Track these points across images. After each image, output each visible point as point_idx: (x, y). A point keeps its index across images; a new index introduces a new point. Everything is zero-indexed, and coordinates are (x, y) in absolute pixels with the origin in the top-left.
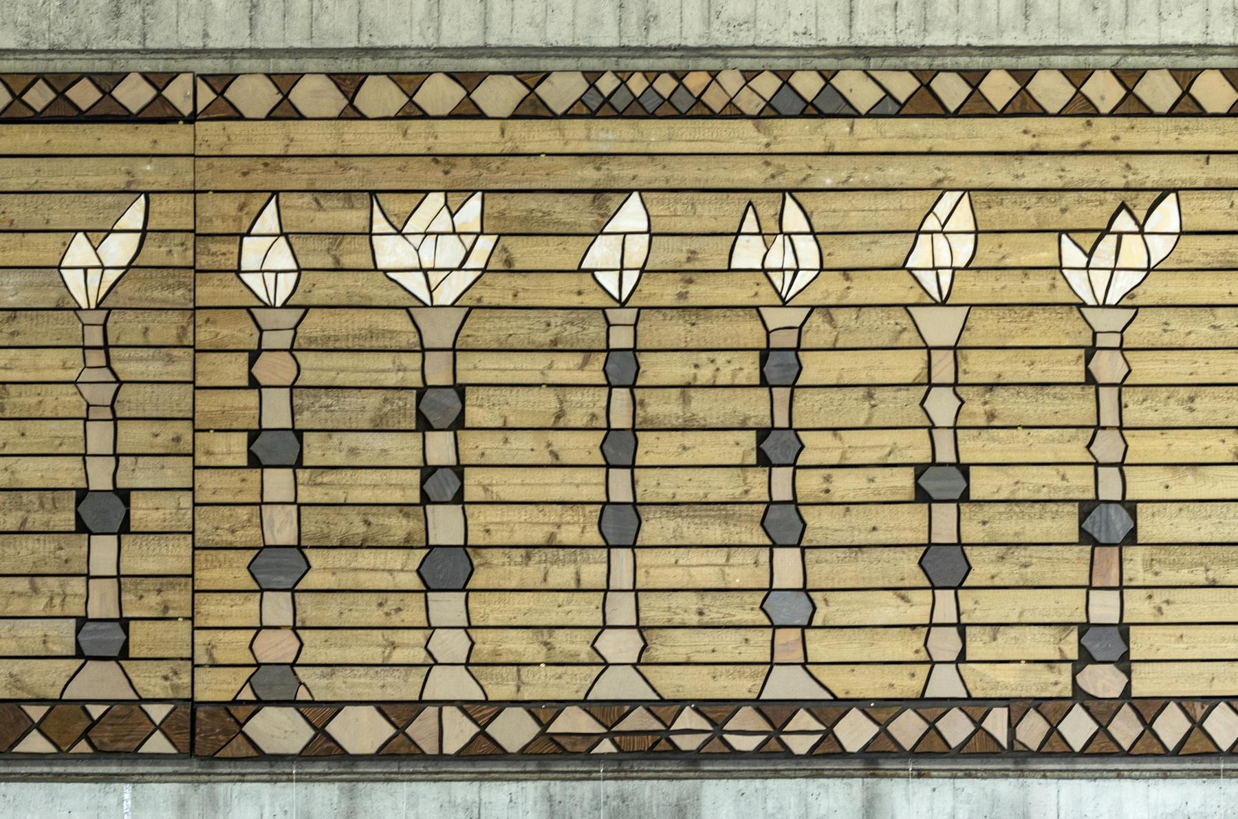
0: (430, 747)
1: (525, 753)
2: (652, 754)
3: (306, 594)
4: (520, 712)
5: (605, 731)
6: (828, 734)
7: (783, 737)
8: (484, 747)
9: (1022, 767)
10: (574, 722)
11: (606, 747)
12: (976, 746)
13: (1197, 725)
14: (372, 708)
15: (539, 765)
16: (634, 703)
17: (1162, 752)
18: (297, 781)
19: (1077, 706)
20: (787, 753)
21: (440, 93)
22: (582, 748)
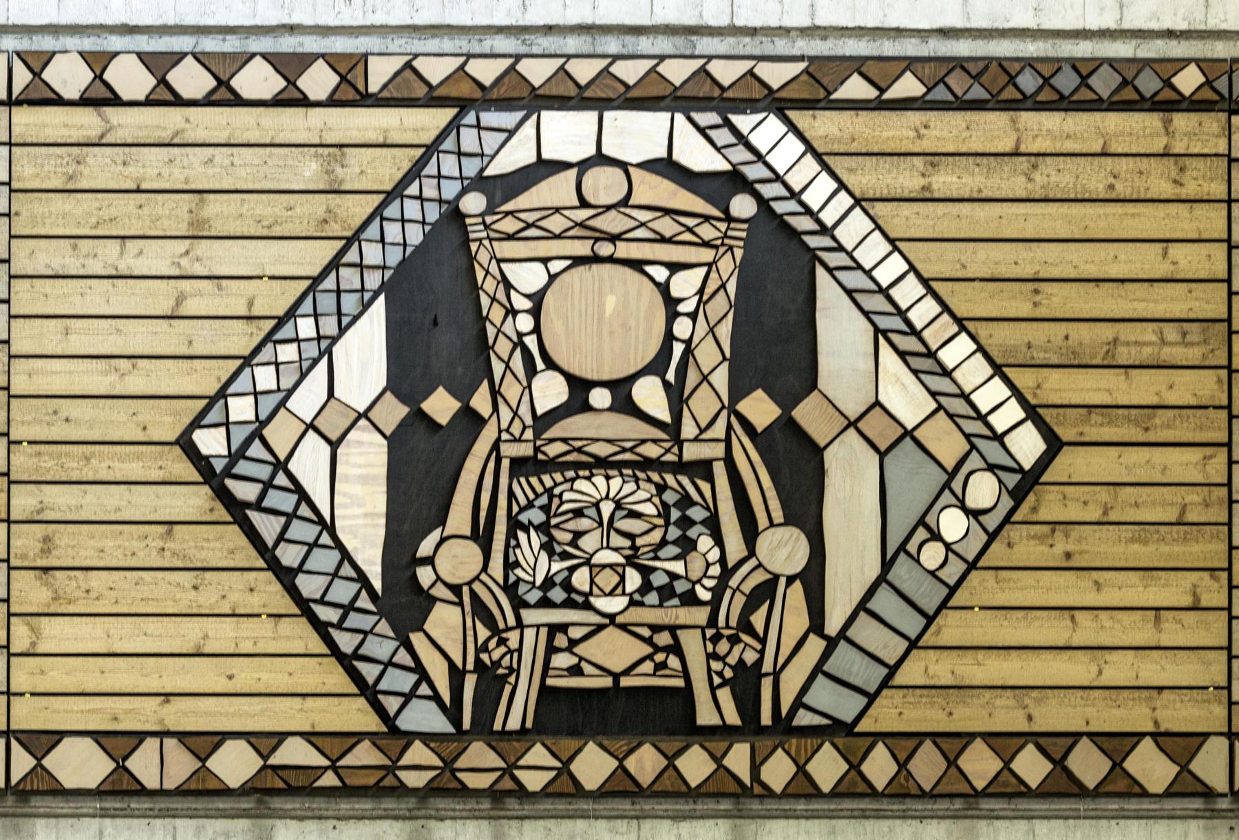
0: (151, 782)
1: (246, 790)
2: (376, 791)
3: (1084, 612)
4: (242, 744)
5: (326, 763)
6: (564, 770)
7: (516, 772)
8: (1121, 785)
9: (1212, 806)
10: (295, 753)
11: (329, 780)
12: (667, 783)
13: (1059, 763)
14: (88, 741)
15: (1206, 803)
16: (359, 736)
17: (572, 789)
18: (1084, 818)
19: (827, 744)
20: (521, 792)
21: (257, 80)
22: (371, 781)
